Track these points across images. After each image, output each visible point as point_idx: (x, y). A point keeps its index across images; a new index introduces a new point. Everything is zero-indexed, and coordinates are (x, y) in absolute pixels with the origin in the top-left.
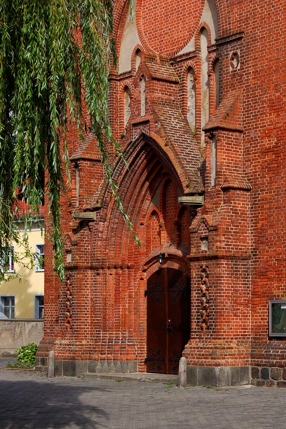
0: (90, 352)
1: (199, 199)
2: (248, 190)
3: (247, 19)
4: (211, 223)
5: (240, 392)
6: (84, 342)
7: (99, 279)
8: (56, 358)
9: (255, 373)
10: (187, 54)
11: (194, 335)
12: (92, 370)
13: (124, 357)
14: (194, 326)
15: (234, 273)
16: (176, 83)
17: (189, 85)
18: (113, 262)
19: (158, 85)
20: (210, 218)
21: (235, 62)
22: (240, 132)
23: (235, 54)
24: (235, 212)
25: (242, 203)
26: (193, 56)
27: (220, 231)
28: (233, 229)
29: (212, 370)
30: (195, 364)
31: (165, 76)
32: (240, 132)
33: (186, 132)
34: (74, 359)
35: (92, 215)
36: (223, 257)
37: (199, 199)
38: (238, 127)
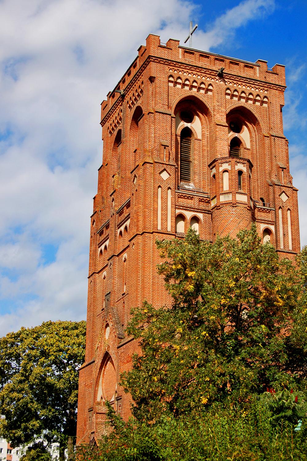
19: (100, 416)
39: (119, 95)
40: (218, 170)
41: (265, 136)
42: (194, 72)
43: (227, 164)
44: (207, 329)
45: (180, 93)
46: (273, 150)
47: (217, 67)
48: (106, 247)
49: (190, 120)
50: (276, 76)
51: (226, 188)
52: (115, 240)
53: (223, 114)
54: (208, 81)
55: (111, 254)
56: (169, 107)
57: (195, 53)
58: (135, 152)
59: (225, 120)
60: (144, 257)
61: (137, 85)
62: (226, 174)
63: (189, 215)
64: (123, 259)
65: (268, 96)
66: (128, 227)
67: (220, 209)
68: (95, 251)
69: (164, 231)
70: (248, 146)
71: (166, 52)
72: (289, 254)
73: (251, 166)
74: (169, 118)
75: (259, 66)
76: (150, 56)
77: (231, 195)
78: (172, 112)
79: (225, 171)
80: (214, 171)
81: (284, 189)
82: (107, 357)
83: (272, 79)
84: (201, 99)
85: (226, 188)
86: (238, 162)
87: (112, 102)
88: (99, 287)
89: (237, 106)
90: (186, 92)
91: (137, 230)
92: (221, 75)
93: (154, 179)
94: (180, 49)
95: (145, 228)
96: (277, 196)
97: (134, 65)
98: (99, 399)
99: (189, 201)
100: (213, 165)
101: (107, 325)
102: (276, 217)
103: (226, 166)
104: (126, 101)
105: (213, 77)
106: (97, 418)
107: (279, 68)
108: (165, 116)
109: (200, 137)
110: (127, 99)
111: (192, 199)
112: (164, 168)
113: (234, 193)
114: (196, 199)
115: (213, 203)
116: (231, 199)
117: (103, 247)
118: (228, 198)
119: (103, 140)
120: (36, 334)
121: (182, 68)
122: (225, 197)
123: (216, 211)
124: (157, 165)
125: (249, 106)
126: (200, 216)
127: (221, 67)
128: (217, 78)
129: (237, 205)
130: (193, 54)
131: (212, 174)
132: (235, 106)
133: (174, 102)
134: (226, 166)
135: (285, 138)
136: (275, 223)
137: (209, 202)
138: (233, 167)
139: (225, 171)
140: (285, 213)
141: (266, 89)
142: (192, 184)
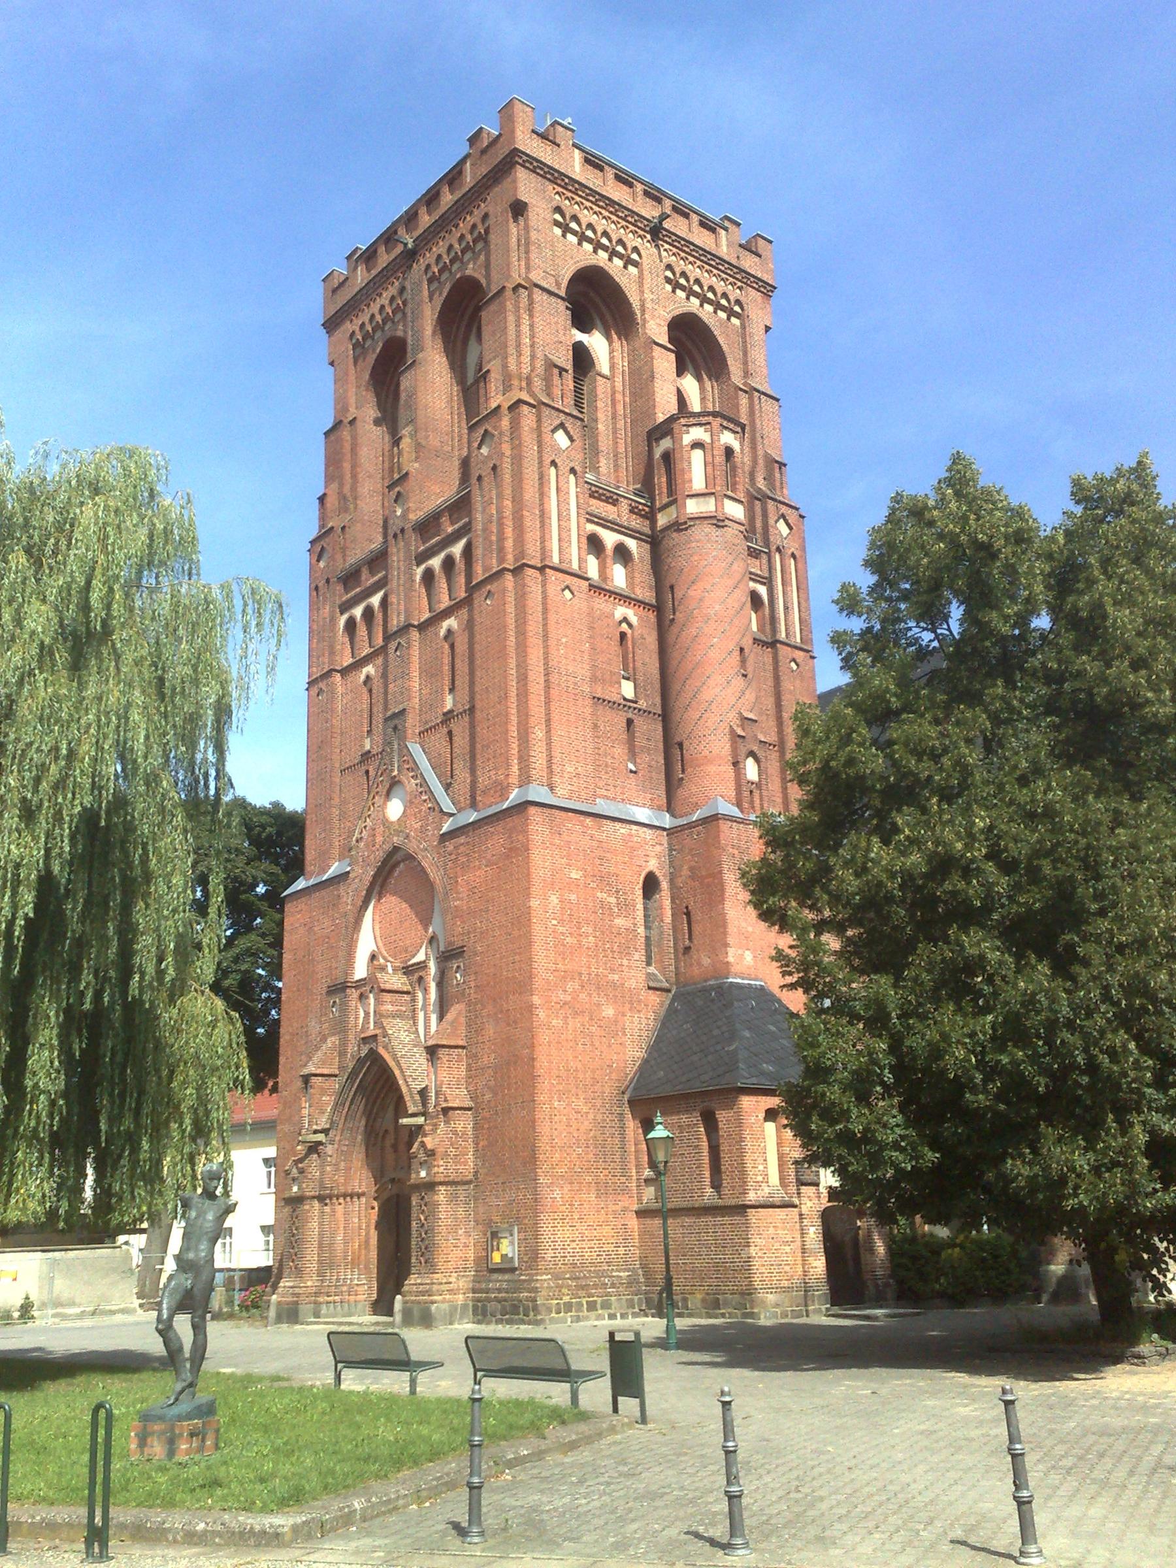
0: (317, 1294)
1: (420, 1120)
2: (469, 1109)
3: (469, 933)
4: (429, 1146)
5: (236, 1366)
6: (309, 1284)
7: (327, 1209)
8: (279, 1303)
9: (475, 1309)
10: (418, 964)
11: (413, 1270)
12: (317, 1315)
13: (352, 1298)
14: (413, 1260)
15: (453, 1199)
16: (408, 993)
17: (420, 995)
18: (342, 1189)
19: (387, 997)
20: (430, 1142)
21: (458, 975)
22: (463, 1047)
23: (458, 967)
24: (455, 1133)
25: (464, 1123)
26: (422, 966)
27: (438, 1155)
28: (452, 1151)
29: (428, 1309)
30: (413, 1302)
31: (395, 987)
32: (463, 1047)
33: (415, 1046)
34: (297, 1303)
35: (321, 1137)
36: (441, 1183)
37: (420, 1120)
38: (461, 1043)
41: (741, 390)
43: (702, 429)
46: (758, 422)
47: (650, 211)
50: (757, 259)
51: (698, 481)
53: (662, 323)
54: (632, 241)
57: (606, 167)
59: (666, 338)
67: (686, 529)
71: (549, 148)
72: (797, 652)
76: (515, 149)
77: (712, 500)
79: (697, 445)
84: (617, 279)
85: (698, 481)
86: (726, 428)
87: (361, 276)
91: (501, 560)
92: (656, 232)
94: (577, 151)
96: (771, 522)
97: (453, 177)
99: (610, 507)
102: (771, 568)
105: (642, 233)
107: (761, 242)
111: (615, 503)
112: (558, 422)
113: (720, 498)
116: (713, 508)
119: (332, 364)
121: (580, 196)
122: (697, 503)
123: (675, 535)
126: (632, 544)
128: (649, 237)
129: (727, 522)
135: (778, 400)
136: (769, 582)
139: (697, 445)
141: (739, 284)
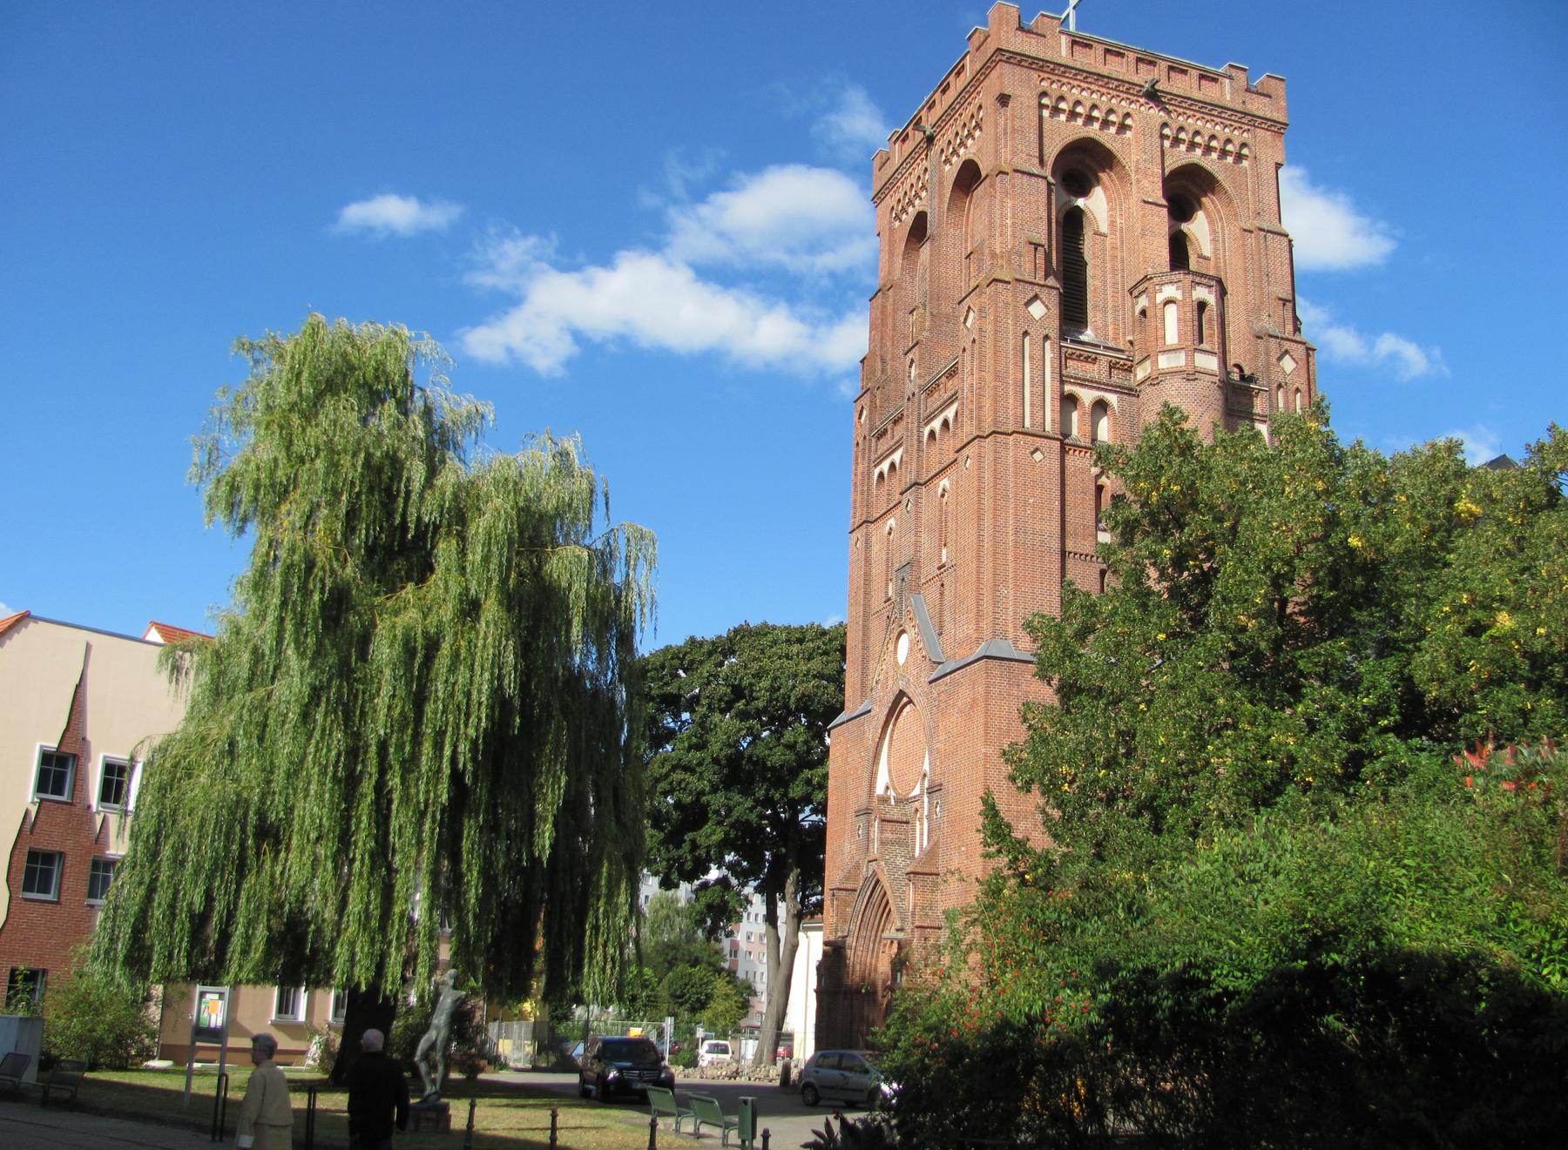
39: (919, 136)
40: (1152, 300)
42: (1093, 87)
44: (1244, 661)
45: (1062, 132)
47: (1144, 76)
48: (893, 466)
49: (1084, 192)
51: (1172, 337)
52: (919, 450)
55: (910, 478)
56: (1042, 162)
58: (968, 257)
59: (1160, 193)
60: (980, 491)
61: (968, 113)
62: (1171, 309)
63: (1087, 396)
64: (940, 491)
65: (1249, 142)
66: (951, 421)
68: (870, 473)
69: (1037, 430)
70: (1207, 250)
73: (1222, 293)
74: (1043, 185)
75: (1230, 78)
77: (1182, 355)
78: (1047, 172)
80: (1143, 302)
81: (1287, 345)
82: (899, 702)
83: (1257, 106)
84: (1108, 146)
85: (1172, 337)
88: (877, 550)
89: (1184, 162)
90: (1078, 130)
91: (979, 428)
92: (1153, 96)
93: (1016, 317)
94: (1063, 37)
95: (995, 422)
98: (880, 790)
99: (1088, 366)
100: (1141, 288)
101: (903, 632)
103: (1170, 291)
104: (936, 149)
106: (882, 831)
108: (1034, 180)
109: (1104, 228)
110: (940, 143)
114: (1103, 363)
115: (1141, 373)
117: (885, 466)
118: (1179, 360)
120: (725, 647)
124: (1021, 286)
125: (1211, 163)
126: (1112, 398)
127: (1150, 78)
128: (1142, 100)
130: (1090, 46)
131: (1138, 309)
132: (1179, 164)
133: (1052, 152)
134: (1170, 291)
137: (1129, 370)
138: (1187, 294)
140: (1291, 398)
142: (1089, 332)
